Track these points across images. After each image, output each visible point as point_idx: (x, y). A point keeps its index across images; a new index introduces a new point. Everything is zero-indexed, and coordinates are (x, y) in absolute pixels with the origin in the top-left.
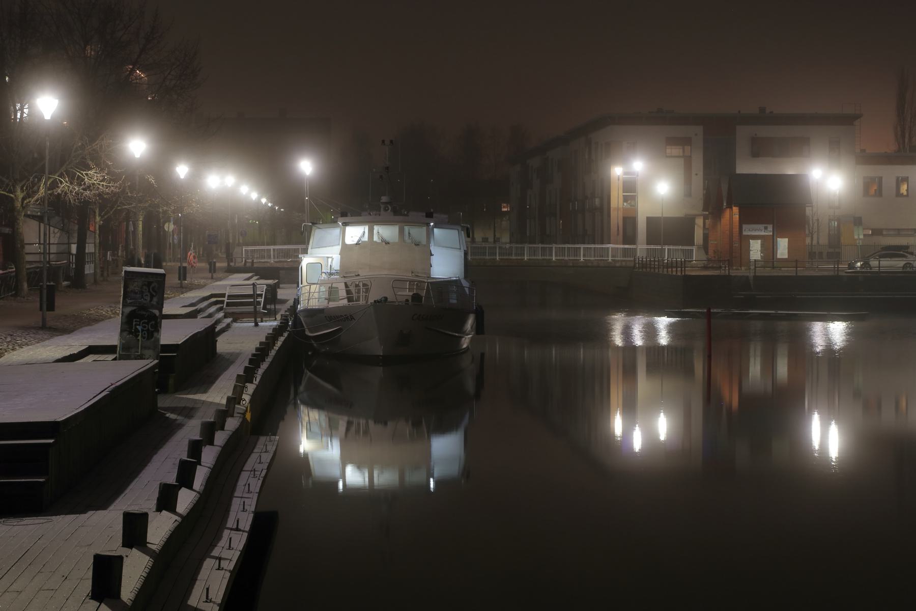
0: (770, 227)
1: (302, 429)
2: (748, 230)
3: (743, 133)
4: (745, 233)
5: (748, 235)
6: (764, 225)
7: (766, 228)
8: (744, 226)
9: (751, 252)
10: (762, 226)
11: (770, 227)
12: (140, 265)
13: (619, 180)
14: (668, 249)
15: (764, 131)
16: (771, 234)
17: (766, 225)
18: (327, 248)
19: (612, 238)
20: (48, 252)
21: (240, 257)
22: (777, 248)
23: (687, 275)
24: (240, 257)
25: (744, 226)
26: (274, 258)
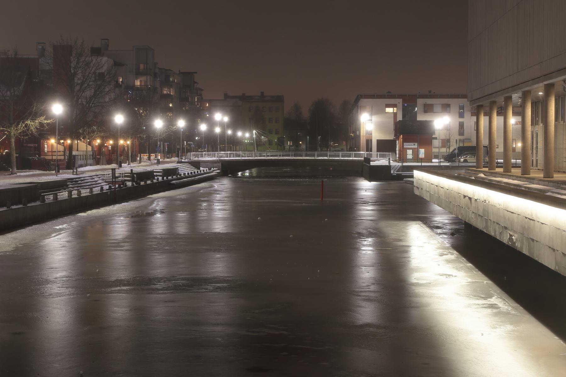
0: (416, 144)
1: (222, 205)
2: (406, 145)
3: (420, 102)
4: (404, 147)
5: (406, 148)
6: (414, 143)
7: (414, 145)
8: (405, 144)
9: (408, 155)
10: (412, 144)
11: (416, 144)
12: (224, 158)
13: (363, 123)
14: (379, 154)
15: (429, 101)
16: (417, 147)
17: (414, 143)
18: (446, 103)
19: (361, 149)
20: (458, 165)
21: (57, 157)
22: (419, 153)
23: (404, 166)
24: (57, 157)
25: (405, 144)
26: (352, 153)
